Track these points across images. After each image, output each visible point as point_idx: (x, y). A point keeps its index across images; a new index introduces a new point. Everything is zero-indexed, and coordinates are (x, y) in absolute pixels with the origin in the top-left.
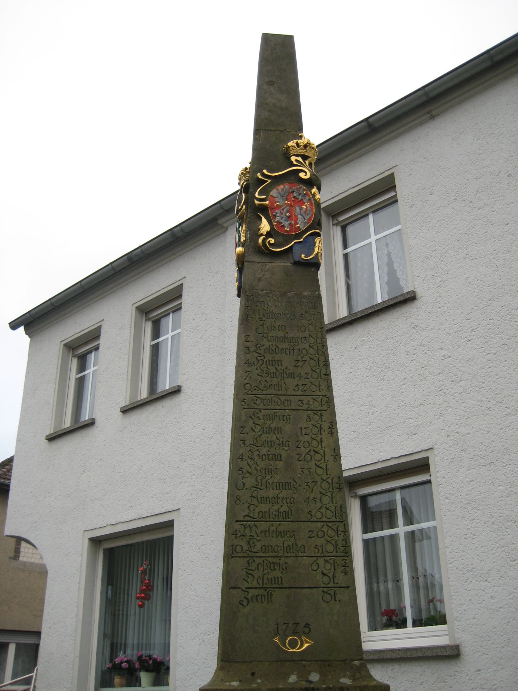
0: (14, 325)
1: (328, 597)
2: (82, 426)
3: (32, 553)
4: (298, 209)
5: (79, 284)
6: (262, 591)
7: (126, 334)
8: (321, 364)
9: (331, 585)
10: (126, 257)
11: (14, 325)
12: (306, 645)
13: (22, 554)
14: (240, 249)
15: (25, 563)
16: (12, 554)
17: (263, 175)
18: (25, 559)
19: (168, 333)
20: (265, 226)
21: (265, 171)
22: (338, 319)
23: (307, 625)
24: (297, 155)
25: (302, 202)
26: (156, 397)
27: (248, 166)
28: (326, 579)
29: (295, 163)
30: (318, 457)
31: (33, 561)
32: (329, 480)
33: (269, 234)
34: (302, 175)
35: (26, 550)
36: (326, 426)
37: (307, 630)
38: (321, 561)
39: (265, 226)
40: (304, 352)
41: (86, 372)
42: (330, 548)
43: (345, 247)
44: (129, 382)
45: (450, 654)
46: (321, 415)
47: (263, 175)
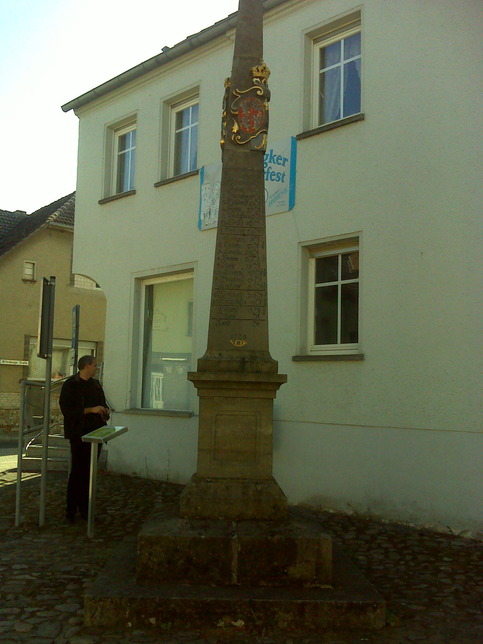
0: (66, 108)
1: (255, 324)
2: (123, 193)
3: (84, 282)
4: (254, 117)
5: (117, 79)
6: (226, 321)
7: (156, 126)
8: (261, 210)
9: (257, 319)
10: (154, 59)
11: (66, 108)
12: (244, 344)
13: (76, 282)
14: (222, 142)
15: (79, 289)
16: (69, 282)
17: (236, 92)
18: (79, 286)
19: (188, 125)
20: (236, 129)
21: (237, 90)
22: (311, 129)
23: (245, 336)
24: (257, 77)
25: (256, 112)
26: (179, 176)
27: (229, 75)
28: (255, 316)
29: (255, 83)
30: (255, 259)
31: (85, 287)
32: (260, 271)
33: (238, 133)
34: (259, 92)
35: (79, 279)
36: (260, 244)
37: (245, 338)
38: (253, 308)
39: (236, 129)
40: (253, 204)
41: (126, 151)
42: (258, 302)
43: (323, 66)
44: (160, 164)
45: (360, 358)
46: (259, 238)
47: (236, 92)
